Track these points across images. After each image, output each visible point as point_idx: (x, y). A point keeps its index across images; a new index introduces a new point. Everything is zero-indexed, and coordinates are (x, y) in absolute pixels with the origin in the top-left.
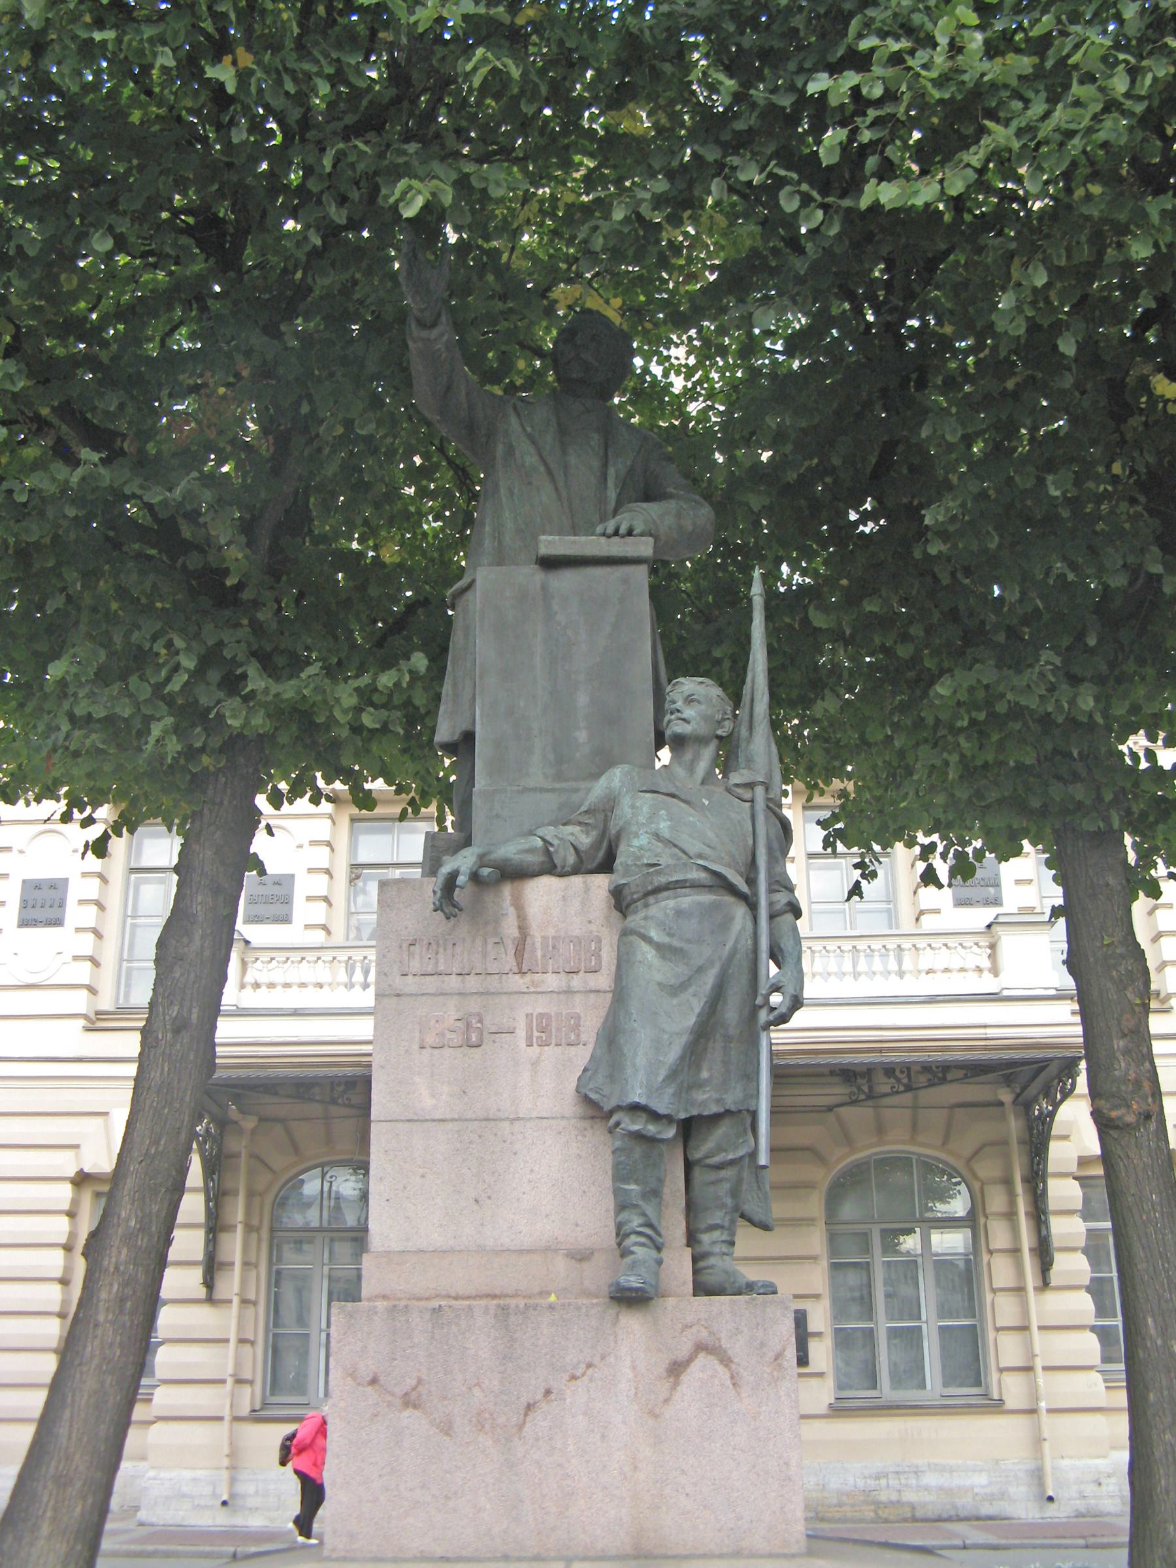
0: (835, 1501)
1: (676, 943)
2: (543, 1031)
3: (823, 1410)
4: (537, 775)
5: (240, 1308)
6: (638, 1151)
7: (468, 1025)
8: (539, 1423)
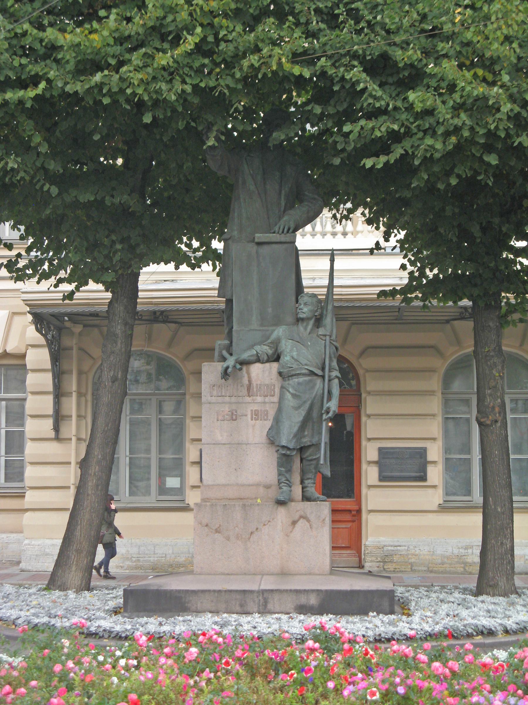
0: (440, 561)
1: (297, 393)
2: (256, 415)
3: (435, 507)
4: (255, 324)
5: (77, 443)
6: (284, 459)
7: (232, 413)
8: (254, 537)
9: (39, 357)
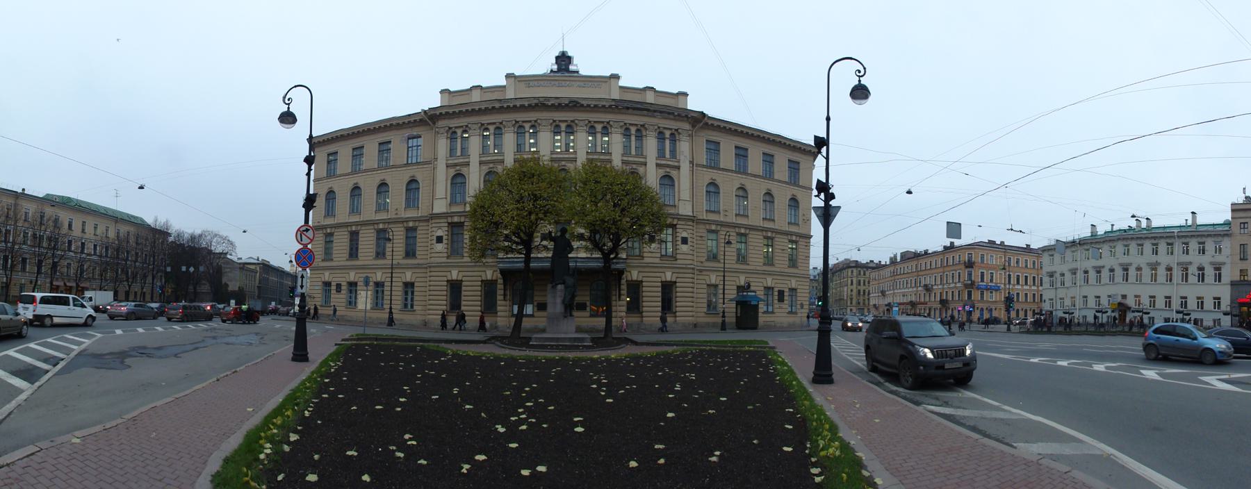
9: (501, 281)
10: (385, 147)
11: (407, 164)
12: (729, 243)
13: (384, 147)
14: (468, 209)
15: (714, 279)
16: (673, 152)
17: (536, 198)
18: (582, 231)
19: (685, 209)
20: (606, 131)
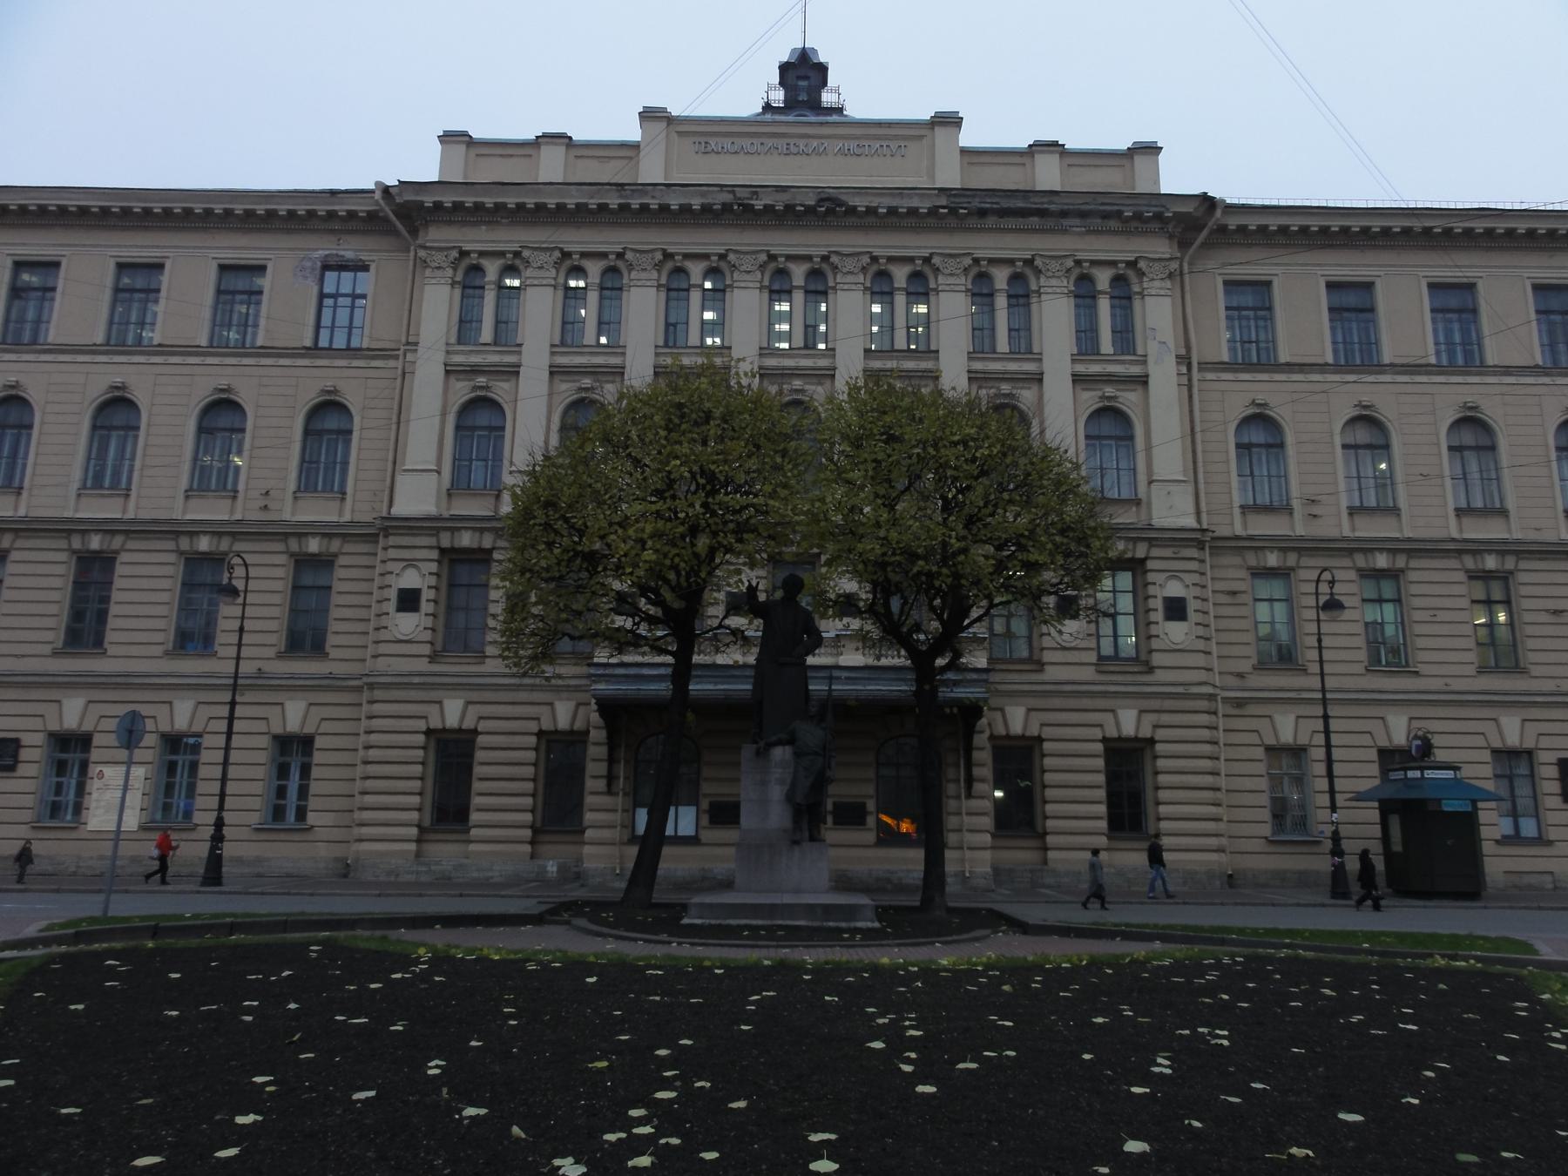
9: (598, 734)
10: (241, 283)
11: (314, 350)
12: (1333, 605)
13: (238, 285)
14: (506, 508)
15: (1286, 728)
16: (1125, 336)
17: (711, 483)
18: (849, 585)
19: (1172, 509)
20: (920, 287)
